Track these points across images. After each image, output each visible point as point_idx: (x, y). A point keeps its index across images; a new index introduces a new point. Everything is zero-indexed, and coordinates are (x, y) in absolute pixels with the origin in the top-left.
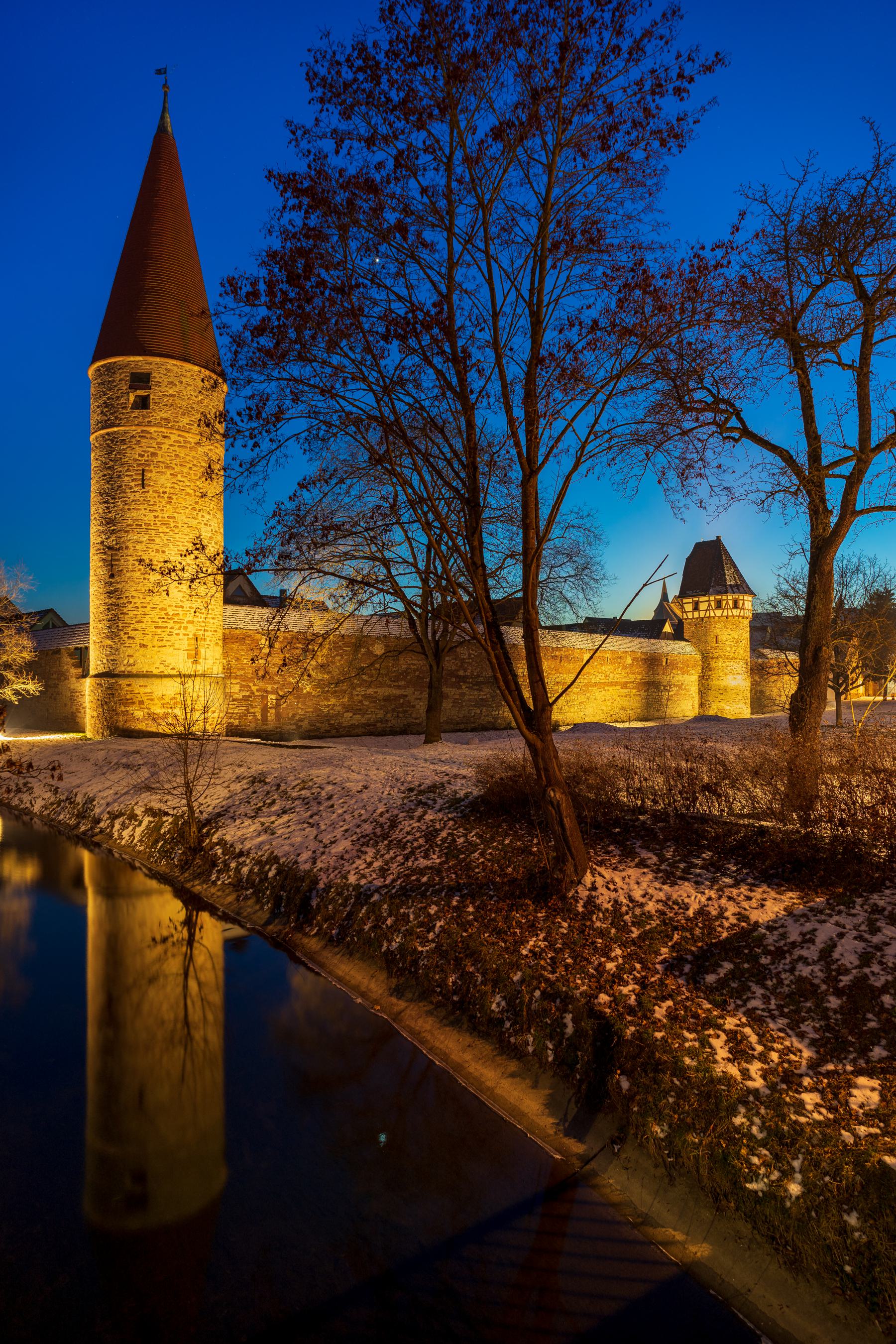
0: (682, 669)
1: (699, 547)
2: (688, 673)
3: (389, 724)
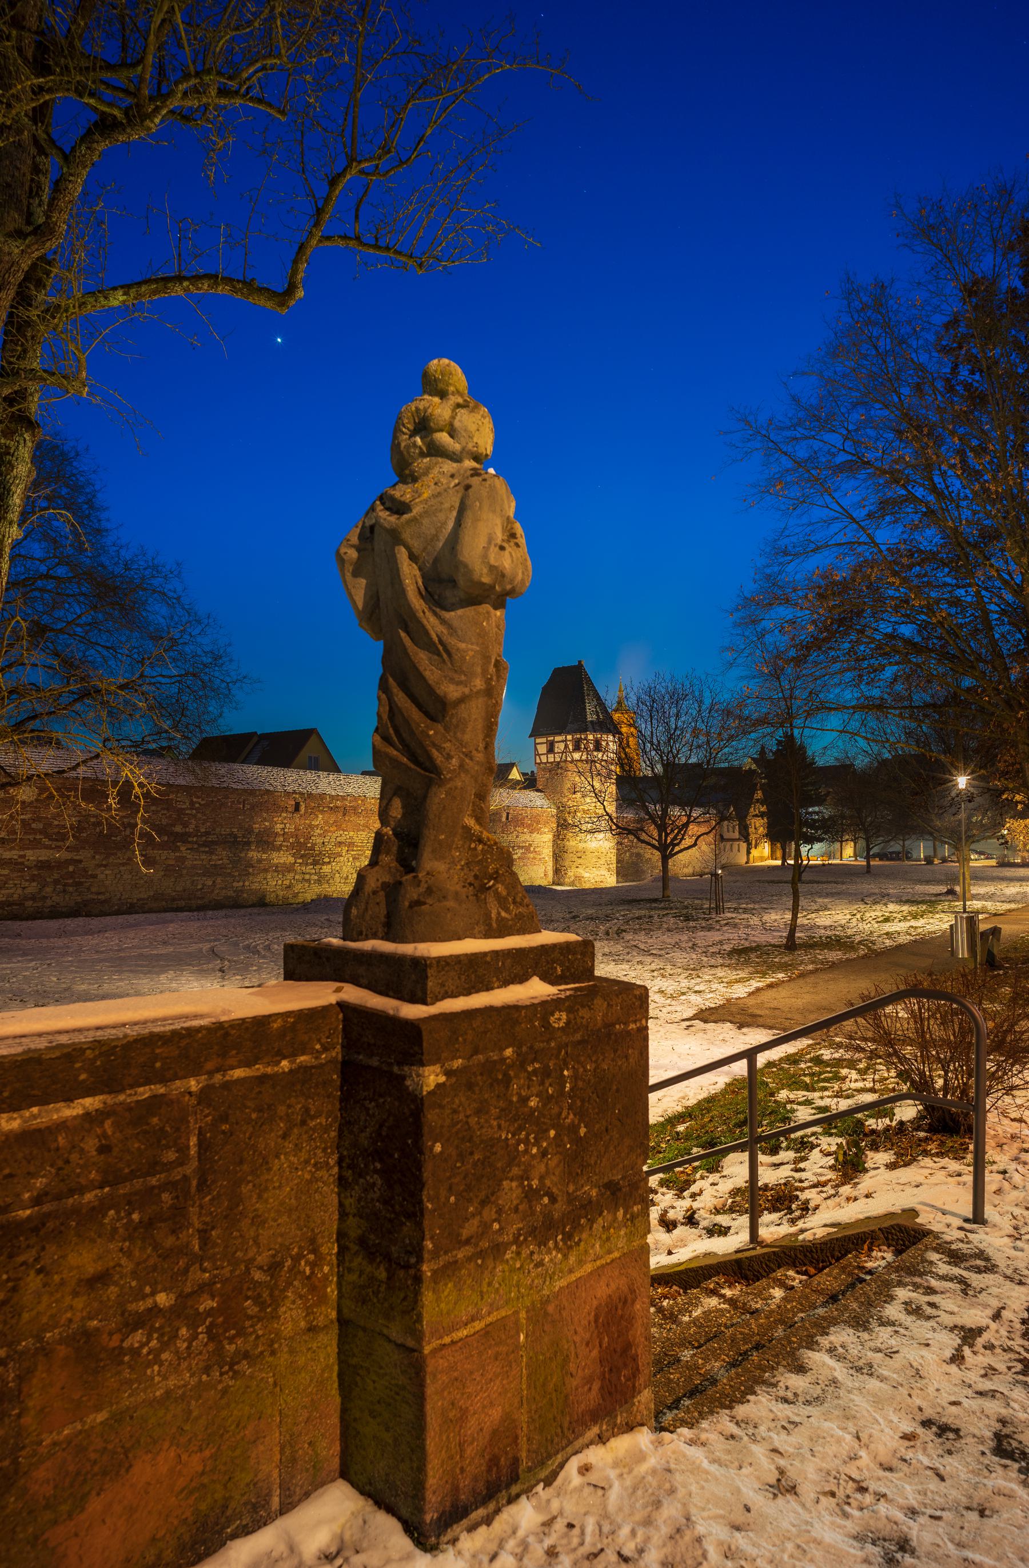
0: (529, 826)
1: (558, 673)
2: (538, 831)
3: (49, 903)
